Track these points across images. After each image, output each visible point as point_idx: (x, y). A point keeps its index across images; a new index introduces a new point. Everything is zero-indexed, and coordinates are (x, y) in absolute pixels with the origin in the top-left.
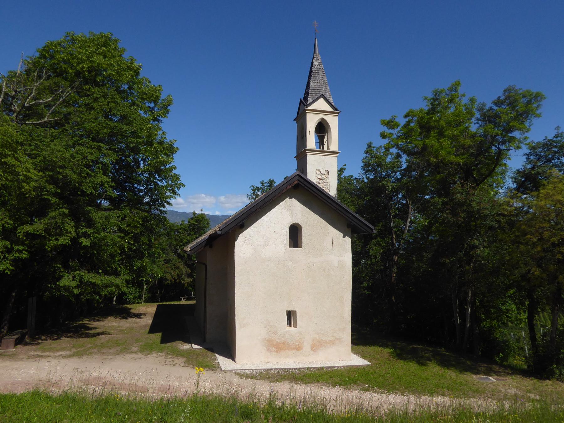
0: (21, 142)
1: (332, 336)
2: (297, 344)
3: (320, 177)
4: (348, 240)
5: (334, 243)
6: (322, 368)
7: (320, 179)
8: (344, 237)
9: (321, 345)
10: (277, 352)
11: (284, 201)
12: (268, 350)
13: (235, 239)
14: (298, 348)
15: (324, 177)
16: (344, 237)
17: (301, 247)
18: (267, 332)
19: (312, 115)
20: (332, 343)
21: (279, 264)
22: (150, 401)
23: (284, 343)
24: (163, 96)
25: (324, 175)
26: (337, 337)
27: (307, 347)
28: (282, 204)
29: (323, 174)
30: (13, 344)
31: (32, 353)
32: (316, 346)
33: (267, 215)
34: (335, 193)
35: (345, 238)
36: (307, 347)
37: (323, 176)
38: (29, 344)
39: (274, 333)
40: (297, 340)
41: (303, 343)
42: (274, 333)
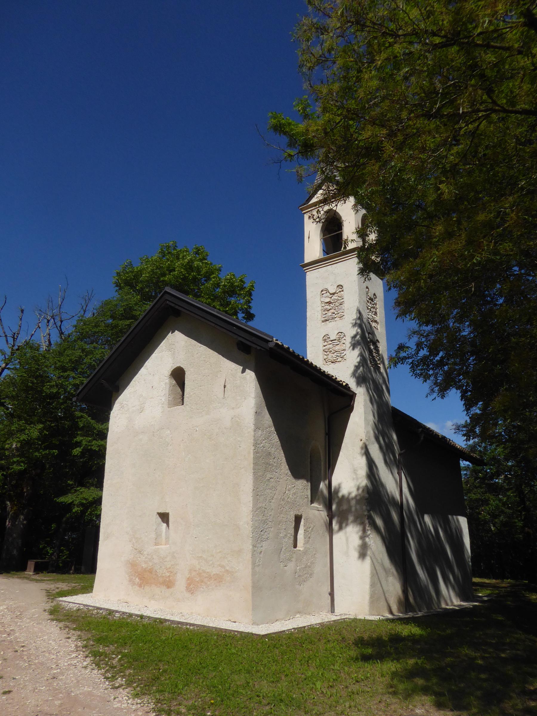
0: (495, 472)
1: (219, 565)
2: (168, 574)
3: (328, 300)
4: (250, 375)
5: (228, 386)
7: (329, 303)
8: (243, 371)
9: (202, 582)
10: (140, 586)
11: (166, 339)
14: (169, 584)
15: (336, 298)
16: (243, 371)
18: (131, 548)
20: (219, 579)
21: (153, 435)
23: (151, 571)
24: (248, 285)
25: (336, 295)
26: (228, 568)
27: (181, 583)
28: (164, 344)
29: (334, 294)
33: (145, 365)
34: (355, 317)
35: (244, 374)
36: (181, 583)
37: (334, 297)
40: (168, 567)
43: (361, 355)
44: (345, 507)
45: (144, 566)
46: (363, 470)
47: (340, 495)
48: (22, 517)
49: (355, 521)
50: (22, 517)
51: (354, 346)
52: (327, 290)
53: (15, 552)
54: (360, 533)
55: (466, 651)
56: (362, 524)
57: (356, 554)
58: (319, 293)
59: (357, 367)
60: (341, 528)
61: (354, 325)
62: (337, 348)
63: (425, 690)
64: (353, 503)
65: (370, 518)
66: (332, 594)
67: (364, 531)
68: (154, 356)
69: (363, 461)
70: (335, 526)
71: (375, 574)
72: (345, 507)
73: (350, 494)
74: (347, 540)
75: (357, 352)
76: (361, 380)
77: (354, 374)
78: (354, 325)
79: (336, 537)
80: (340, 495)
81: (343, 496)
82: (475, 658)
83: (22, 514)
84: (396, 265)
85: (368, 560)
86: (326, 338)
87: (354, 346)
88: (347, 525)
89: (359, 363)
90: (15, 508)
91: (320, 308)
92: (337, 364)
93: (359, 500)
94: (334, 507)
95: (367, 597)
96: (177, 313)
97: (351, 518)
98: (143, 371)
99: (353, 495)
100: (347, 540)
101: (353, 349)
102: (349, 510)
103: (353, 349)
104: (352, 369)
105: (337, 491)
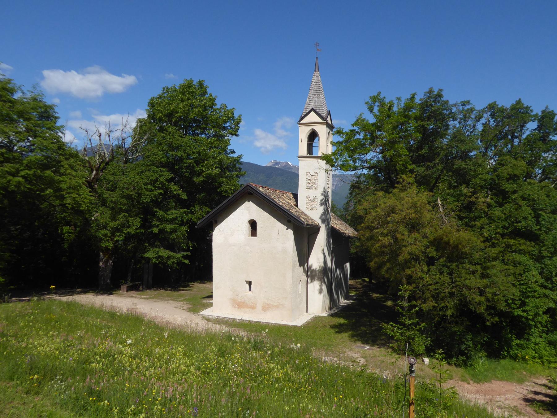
3: (310, 178)
5: (279, 234)
6: (259, 322)
7: (310, 180)
8: (287, 229)
10: (238, 308)
12: (233, 306)
13: (212, 230)
14: (253, 308)
16: (287, 229)
17: (256, 236)
19: (303, 127)
20: (277, 307)
22: (263, 345)
23: (243, 303)
27: (259, 307)
28: (243, 206)
30: (125, 290)
31: (180, 299)
32: (265, 308)
36: (259, 307)
37: (313, 177)
38: (142, 291)
39: (237, 295)
41: (256, 304)
42: (237, 295)
43: (324, 209)
44: (314, 274)
45: (240, 301)
46: (322, 260)
47: (312, 269)
48: (111, 261)
49: (318, 279)
50: (111, 261)
51: (321, 205)
52: (310, 173)
53: (108, 281)
54: (320, 284)
55: (363, 328)
56: (320, 280)
57: (318, 292)
58: (305, 174)
59: (322, 215)
60: (312, 282)
61: (322, 194)
62: (313, 203)
63: (358, 340)
64: (317, 272)
65: (323, 278)
66: (307, 306)
67: (321, 283)
68: (238, 210)
69: (322, 256)
70: (309, 281)
71: (324, 299)
72: (314, 274)
73: (316, 269)
74: (314, 287)
75: (322, 208)
76: (323, 221)
77: (321, 218)
78: (322, 194)
79: (309, 285)
80: (312, 269)
81: (313, 269)
82: (366, 330)
83: (111, 260)
84: (343, 167)
85: (322, 294)
86: (308, 197)
87: (321, 205)
88: (314, 281)
89: (323, 213)
90: (107, 257)
91: (306, 181)
92: (313, 211)
93: (320, 271)
94: (309, 273)
95: (321, 307)
96: (251, 194)
97: (316, 278)
98: (231, 217)
99: (318, 269)
100: (314, 287)
101: (321, 206)
102: (315, 275)
103: (321, 206)
104: (320, 215)
105: (311, 267)
